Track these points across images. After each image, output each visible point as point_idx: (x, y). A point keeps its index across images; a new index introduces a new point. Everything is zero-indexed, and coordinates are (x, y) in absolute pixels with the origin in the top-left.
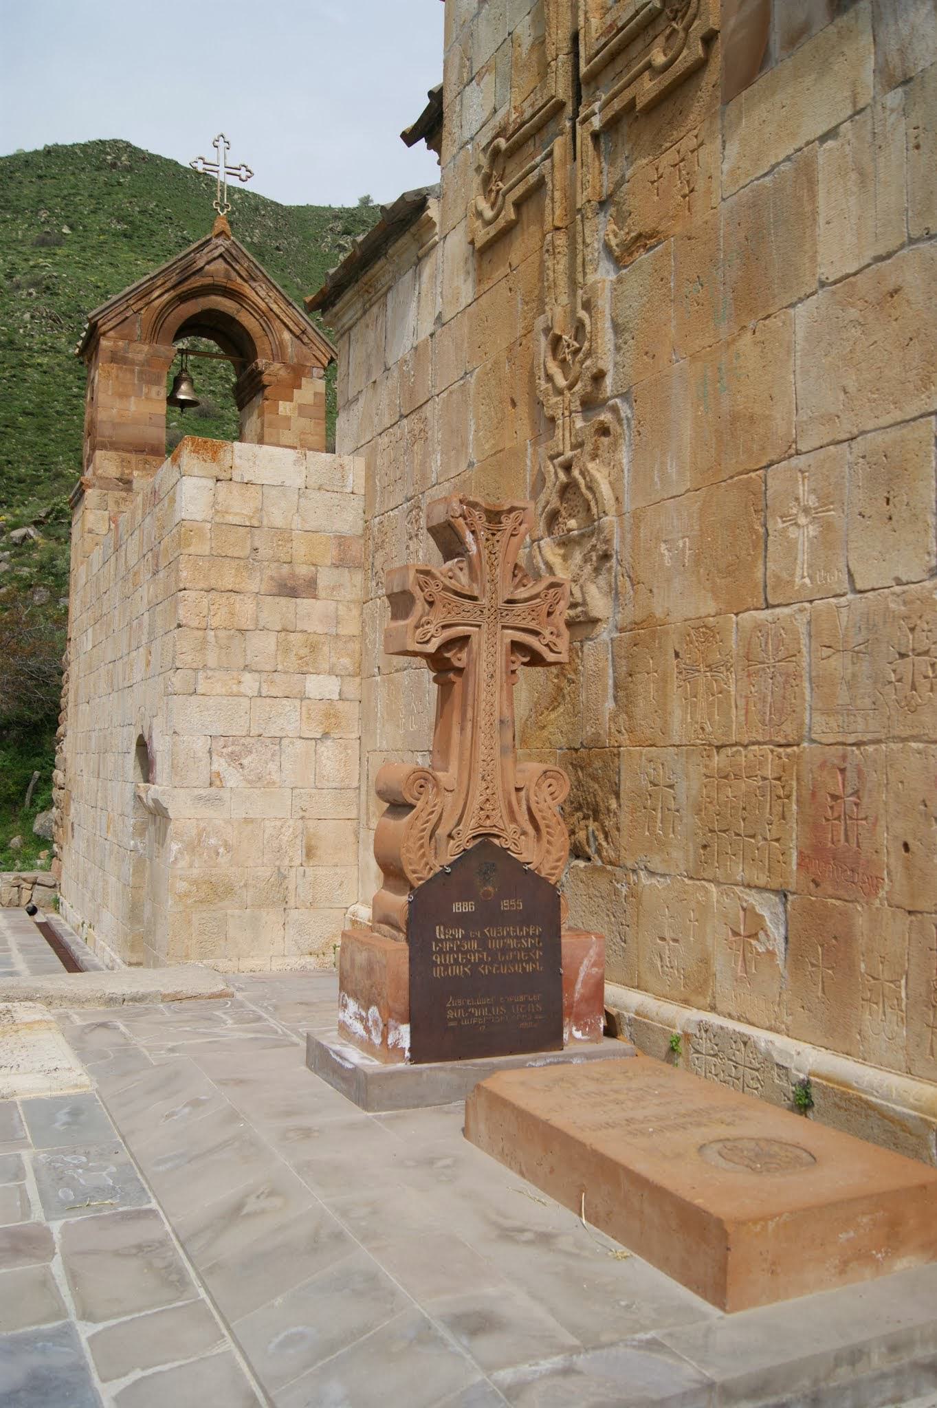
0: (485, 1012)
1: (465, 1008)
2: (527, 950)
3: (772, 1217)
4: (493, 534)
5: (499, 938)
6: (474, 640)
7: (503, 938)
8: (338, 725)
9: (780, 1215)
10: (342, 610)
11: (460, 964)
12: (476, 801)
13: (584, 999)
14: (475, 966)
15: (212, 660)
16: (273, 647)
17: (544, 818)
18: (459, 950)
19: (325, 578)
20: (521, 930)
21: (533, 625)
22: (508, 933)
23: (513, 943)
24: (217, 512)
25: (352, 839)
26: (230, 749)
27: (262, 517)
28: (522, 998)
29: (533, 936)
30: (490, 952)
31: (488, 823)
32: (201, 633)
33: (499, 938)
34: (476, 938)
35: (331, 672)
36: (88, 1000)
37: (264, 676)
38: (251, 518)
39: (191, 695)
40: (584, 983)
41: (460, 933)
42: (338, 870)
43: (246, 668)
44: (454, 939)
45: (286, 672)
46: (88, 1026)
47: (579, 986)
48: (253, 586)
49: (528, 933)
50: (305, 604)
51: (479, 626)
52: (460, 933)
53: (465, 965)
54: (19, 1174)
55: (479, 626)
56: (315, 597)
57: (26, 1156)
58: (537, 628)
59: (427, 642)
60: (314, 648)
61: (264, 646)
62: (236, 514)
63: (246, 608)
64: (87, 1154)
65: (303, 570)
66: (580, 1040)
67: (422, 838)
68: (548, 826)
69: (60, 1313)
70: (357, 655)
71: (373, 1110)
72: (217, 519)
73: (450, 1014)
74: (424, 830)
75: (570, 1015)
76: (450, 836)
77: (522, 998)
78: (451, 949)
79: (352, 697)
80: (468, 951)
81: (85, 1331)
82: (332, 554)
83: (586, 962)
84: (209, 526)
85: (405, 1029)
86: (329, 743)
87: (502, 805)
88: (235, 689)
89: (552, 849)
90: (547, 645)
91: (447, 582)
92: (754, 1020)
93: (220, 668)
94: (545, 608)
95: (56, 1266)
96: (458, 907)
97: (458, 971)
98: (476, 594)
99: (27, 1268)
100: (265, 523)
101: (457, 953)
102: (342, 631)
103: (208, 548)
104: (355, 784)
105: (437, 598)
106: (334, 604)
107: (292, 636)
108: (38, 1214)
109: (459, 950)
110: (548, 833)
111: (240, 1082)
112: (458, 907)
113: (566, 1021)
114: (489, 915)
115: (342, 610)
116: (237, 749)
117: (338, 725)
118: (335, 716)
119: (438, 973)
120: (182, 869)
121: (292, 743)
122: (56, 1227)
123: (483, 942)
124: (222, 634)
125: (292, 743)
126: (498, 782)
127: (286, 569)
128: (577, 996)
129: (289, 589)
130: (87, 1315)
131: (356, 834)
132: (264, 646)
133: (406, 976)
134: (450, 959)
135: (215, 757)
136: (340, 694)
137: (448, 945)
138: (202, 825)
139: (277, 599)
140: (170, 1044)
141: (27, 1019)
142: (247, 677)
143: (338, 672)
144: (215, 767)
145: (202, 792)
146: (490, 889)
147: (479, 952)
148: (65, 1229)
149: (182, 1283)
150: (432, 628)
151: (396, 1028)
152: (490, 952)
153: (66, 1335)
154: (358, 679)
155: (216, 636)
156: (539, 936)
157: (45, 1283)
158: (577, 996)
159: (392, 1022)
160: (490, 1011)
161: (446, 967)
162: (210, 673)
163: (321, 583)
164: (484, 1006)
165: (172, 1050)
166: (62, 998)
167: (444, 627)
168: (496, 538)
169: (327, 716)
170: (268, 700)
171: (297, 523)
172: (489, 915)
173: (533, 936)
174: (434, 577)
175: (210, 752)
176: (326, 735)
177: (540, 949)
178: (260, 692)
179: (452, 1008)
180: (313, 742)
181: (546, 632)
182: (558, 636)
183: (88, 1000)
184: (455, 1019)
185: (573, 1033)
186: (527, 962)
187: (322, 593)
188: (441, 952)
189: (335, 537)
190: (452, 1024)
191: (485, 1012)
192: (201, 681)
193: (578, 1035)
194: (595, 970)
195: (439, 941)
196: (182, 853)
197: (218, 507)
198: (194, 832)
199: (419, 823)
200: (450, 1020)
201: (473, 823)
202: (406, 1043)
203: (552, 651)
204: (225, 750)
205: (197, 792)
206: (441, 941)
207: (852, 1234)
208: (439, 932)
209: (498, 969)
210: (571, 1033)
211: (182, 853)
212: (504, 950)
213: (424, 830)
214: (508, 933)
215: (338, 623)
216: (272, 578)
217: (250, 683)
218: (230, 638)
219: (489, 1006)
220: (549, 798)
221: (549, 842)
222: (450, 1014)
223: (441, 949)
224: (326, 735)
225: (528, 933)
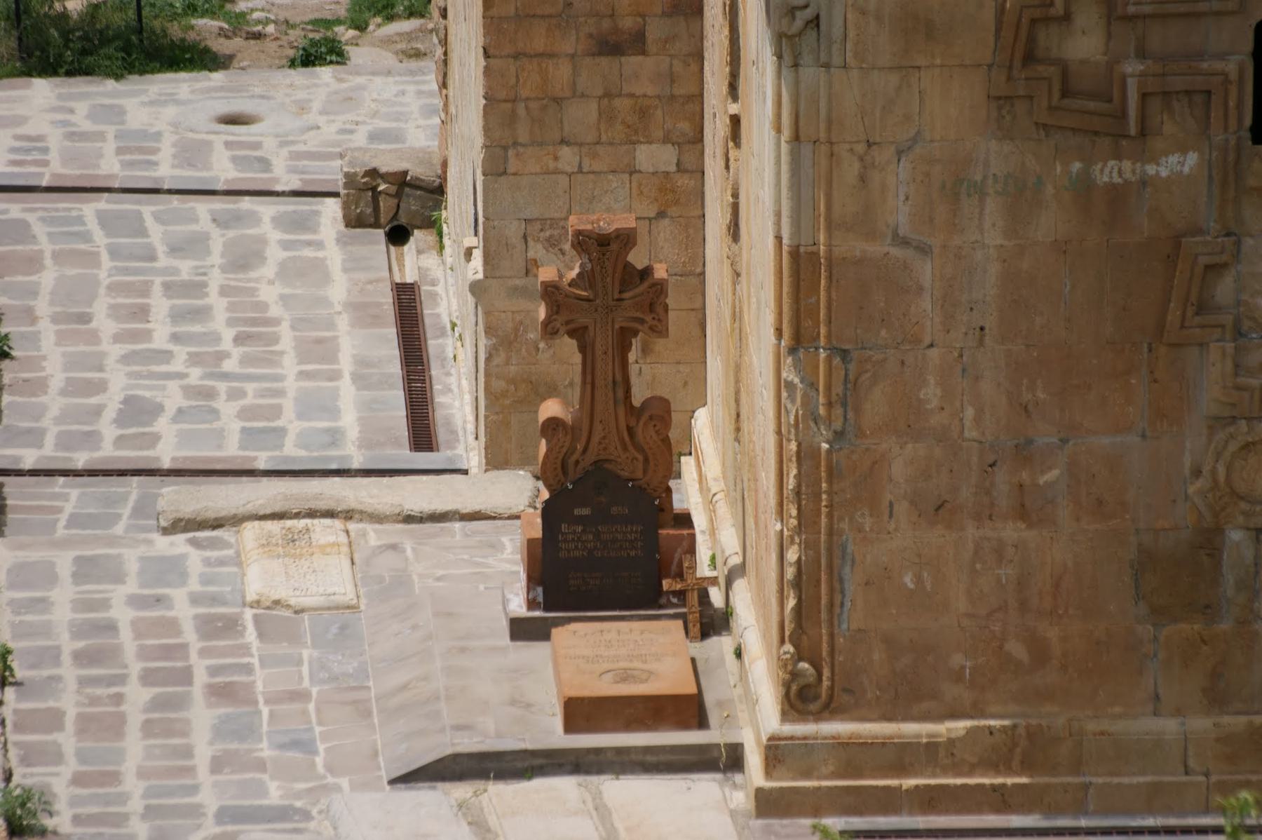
10: (678, 66)
12: (596, 439)
15: (523, 134)
16: (595, 114)
19: (655, 30)
21: (638, 315)
23: (619, 536)
26: (548, 234)
32: (509, 105)
35: (666, 140)
37: (585, 149)
39: (500, 175)
41: (580, 529)
42: (681, 368)
43: (563, 142)
45: (611, 144)
46: (380, 547)
48: (568, 46)
50: (632, 62)
52: (580, 529)
54: (299, 662)
56: (643, 53)
57: (306, 653)
60: (644, 113)
61: (581, 116)
63: (561, 72)
64: (343, 655)
65: (627, 23)
69: (310, 722)
81: (318, 729)
83: (679, 550)
85: (540, 590)
86: (666, 222)
88: (552, 165)
92: (326, 614)
93: (533, 143)
95: (311, 707)
96: (577, 512)
97: (577, 553)
99: (296, 706)
102: (677, 92)
106: (668, 59)
107: (617, 102)
108: (306, 683)
111: (449, 614)
112: (577, 512)
115: (678, 66)
116: (556, 232)
118: (673, 191)
119: (562, 554)
120: (497, 366)
122: (314, 691)
124: (533, 105)
127: (606, 24)
129: (613, 45)
130: (320, 723)
132: (581, 116)
135: (531, 243)
136: (678, 165)
138: (518, 318)
139: (598, 60)
140: (441, 573)
141: (322, 542)
142: (565, 151)
143: (675, 139)
144: (531, 254)
145: (517, 282)
148: (318, 693)
149: (369, 714)
153: (311, 730)
154: (673, 168)
155: (527, 108)
157: (305, 712)
162: (521, 150)
163: (650, 37)
165: (439, 579)
166: (361, 512)
170: (591, 176)
175: (525, 237)
176: (661, 215)
178: (580, 166)
187: (651, 46)
188: (565, 541)
196: (497, 350)
198: (510, 325)
204: (542, 234)
205: (511, 283)
211: (497, 350)
215: (673, 81)
216: (591, 36)
217: (568, 157)
218: (544, 108)
222: (572, 582)
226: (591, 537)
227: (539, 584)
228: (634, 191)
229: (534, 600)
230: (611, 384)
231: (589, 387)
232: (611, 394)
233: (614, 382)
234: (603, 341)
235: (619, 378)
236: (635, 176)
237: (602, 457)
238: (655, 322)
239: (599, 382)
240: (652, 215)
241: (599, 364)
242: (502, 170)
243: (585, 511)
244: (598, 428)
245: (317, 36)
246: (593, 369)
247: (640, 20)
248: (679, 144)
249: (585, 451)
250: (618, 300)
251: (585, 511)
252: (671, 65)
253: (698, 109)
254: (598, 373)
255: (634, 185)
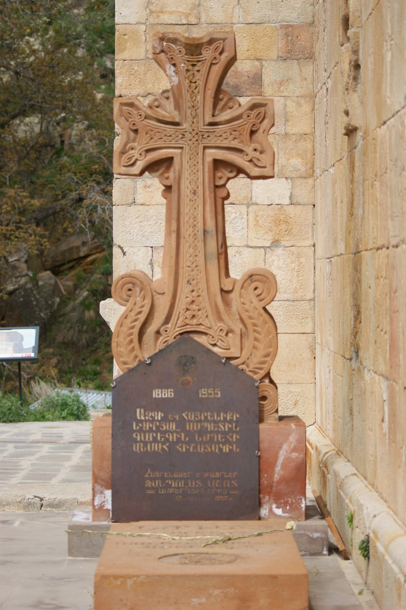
0: (182, 484)
1: (163, 479)
2: (224, 433)
3: (130, 577)
4: (194, 65)
5: (197, 422)
6: (176, 161)
7: (200, 421)
8: (289, 231)
9: (138, 576)
11: (158, 442)
12: (180, 306)
13: (283, 480)
14: (172, 445)
17: (250, 318)
18: (158, 430)
20: (219, 415)
21: (234, 144)
22: (206, 418)
23: (210, 427)
24: (152, 12)
25: (307, 354)
27: (199, 13)
28: (218, 475)
29: (230, 422)
30: (188, 433)
31: (195, 321)
33: (197, 422)
34: (174, 420)
36: (8, 504)
38: (187, 16)
39: (130, 205)
40: (284, 466)
41: (159, 416)
44: (153, 420)
47: (278, 468)
49: (225, 419)
51: (182, 148)
52: (159, 416)
53: (163, 443)
55: (182, 148)
58: (240, 146)
59: (133, 165)
62: (171, 13)
66: (280, 516)
67: (131, 334)
68: (255, 325)
70: (309, 155)
71: (75, 556)
72: (151, 20)
73: (149, 484)
74: (133, 328)
75: (269, 493)
76: (158, 333)
77: (218, 475)
78: (151, 429)
79: (306, 200)
80: (166, 432)
82: (278, 46)
83: (285, 446)
84: (143, 27)
85: (108, 493)
86: (279, 251)
87: (206, 304)
89: (261, 346)
90: (251, 161)
91: (149, 112)
94: (248, 128)
96: (157, 394)
97: (156, 447)
98: (177, 120)
100: (203, 20)
101: (156, 432)
102: (291, 130)
103: (143, 50)
104: (310, 296)
105: (139, 126)
109: (158, 430)
110: (255, 331)
112: (157, 394)
113: (266, 499)
114: (187, 400)
117: (289, 231)
119: (137, 448)
121: (239, 253)
123: (181, 424)
125: (239, 253)
126: (203, 285)
128: (276, 477)
131: (313, 350)
133: (109, 450)
134: (149, 437)
136: (291, 198)
137: (147, 426)
143: (288, 174)
146: (189, 378)
147: (177, 433)
150: (135, 153)
151: (102, 492)
152: (188, 433)
154: (287, 201)
156: (237, 422)
158: (276, 477)
159: (98, 487)
160: (186, 484)
161: (145, 444)
163: (266, 80)
164: (181, 479)
167: (148, 151)
168: (196, 68)
169: (277, 222)
171: (238, 15)
172: (187, 400)
173: (230, 422)
174: (138, 108)
176: (276, 243)
177: (237, 433)
179: (151, 479)
180: (262, 251)
181: (249, 149)
182: (261, 153)
183: (8, 504)
184: (152, 488)
185: (270, 509)
186: (224, 444)
188: (141, 430)
189: (282, 27)
190: (150, 492)
191: (182, 484)
192: (140, 190)
193: (279, 512)
194: (294, 455)
195: (139, 422)
197: (153, 8)
199: (129, 321)
200: (148, 488)
201: (180, 323)
202: (109, 506)
203: (256, 166)
206: (141, 421)
207: (204, 600)
208: (140, 414)
209: (195, 448)
210: (271, 510)
212: (202, 432)
213: (133, 328)
214: (206, 418)
215: (287, 121)
219: (186, 480)
220: (255, 300)
221: (256, 339)
222: (149, 484)
223: (141, 428)
224: (276, 243)
225: (225, 419)
226: (173, 426)
227: (107, 488)
228: (252, 222)
229: (101, 507)
230: (201, 233)
231: (174, 236)
232: (201, 244)
233: (205, 232)
234: (192, 173)
235: (211, 224)
236: (252, 208)
237: (189, 328)
238: (257, 154)
239: (186, 231)
240: (268, 244)
241: (186, 209)
242: (131, 200)
243: (167, 394)
244: (184, 290)
245: (95, 345)
246: (207, 281)
247: (257, 63)
248: (292, 179)
249: (167, 320)
250: (211, 124)
251: (167, 394)
252: (285, 105)
253: (309, 146)
254: (185, 219)
255: (251, 216)
